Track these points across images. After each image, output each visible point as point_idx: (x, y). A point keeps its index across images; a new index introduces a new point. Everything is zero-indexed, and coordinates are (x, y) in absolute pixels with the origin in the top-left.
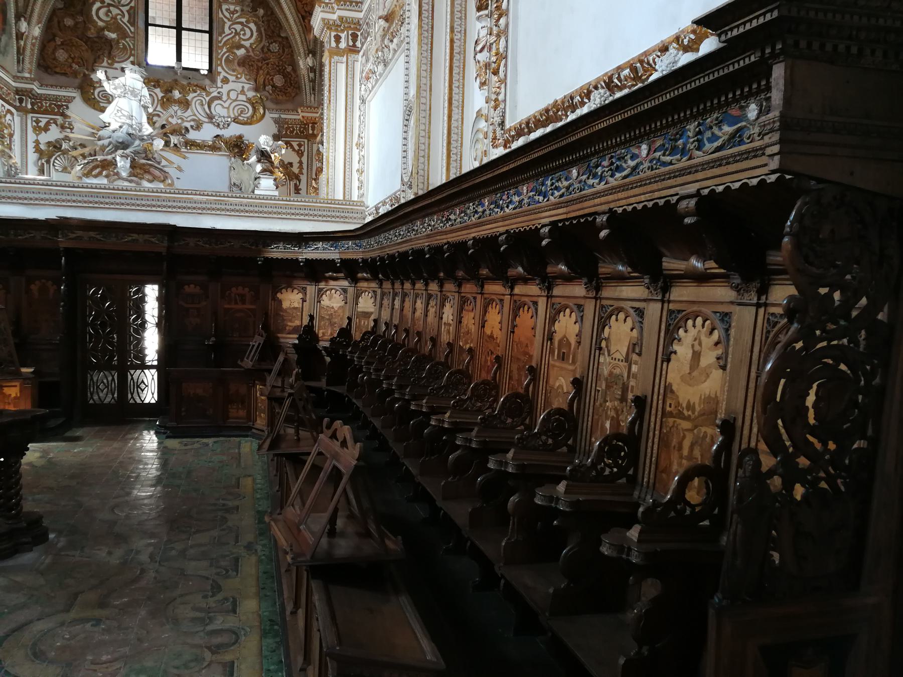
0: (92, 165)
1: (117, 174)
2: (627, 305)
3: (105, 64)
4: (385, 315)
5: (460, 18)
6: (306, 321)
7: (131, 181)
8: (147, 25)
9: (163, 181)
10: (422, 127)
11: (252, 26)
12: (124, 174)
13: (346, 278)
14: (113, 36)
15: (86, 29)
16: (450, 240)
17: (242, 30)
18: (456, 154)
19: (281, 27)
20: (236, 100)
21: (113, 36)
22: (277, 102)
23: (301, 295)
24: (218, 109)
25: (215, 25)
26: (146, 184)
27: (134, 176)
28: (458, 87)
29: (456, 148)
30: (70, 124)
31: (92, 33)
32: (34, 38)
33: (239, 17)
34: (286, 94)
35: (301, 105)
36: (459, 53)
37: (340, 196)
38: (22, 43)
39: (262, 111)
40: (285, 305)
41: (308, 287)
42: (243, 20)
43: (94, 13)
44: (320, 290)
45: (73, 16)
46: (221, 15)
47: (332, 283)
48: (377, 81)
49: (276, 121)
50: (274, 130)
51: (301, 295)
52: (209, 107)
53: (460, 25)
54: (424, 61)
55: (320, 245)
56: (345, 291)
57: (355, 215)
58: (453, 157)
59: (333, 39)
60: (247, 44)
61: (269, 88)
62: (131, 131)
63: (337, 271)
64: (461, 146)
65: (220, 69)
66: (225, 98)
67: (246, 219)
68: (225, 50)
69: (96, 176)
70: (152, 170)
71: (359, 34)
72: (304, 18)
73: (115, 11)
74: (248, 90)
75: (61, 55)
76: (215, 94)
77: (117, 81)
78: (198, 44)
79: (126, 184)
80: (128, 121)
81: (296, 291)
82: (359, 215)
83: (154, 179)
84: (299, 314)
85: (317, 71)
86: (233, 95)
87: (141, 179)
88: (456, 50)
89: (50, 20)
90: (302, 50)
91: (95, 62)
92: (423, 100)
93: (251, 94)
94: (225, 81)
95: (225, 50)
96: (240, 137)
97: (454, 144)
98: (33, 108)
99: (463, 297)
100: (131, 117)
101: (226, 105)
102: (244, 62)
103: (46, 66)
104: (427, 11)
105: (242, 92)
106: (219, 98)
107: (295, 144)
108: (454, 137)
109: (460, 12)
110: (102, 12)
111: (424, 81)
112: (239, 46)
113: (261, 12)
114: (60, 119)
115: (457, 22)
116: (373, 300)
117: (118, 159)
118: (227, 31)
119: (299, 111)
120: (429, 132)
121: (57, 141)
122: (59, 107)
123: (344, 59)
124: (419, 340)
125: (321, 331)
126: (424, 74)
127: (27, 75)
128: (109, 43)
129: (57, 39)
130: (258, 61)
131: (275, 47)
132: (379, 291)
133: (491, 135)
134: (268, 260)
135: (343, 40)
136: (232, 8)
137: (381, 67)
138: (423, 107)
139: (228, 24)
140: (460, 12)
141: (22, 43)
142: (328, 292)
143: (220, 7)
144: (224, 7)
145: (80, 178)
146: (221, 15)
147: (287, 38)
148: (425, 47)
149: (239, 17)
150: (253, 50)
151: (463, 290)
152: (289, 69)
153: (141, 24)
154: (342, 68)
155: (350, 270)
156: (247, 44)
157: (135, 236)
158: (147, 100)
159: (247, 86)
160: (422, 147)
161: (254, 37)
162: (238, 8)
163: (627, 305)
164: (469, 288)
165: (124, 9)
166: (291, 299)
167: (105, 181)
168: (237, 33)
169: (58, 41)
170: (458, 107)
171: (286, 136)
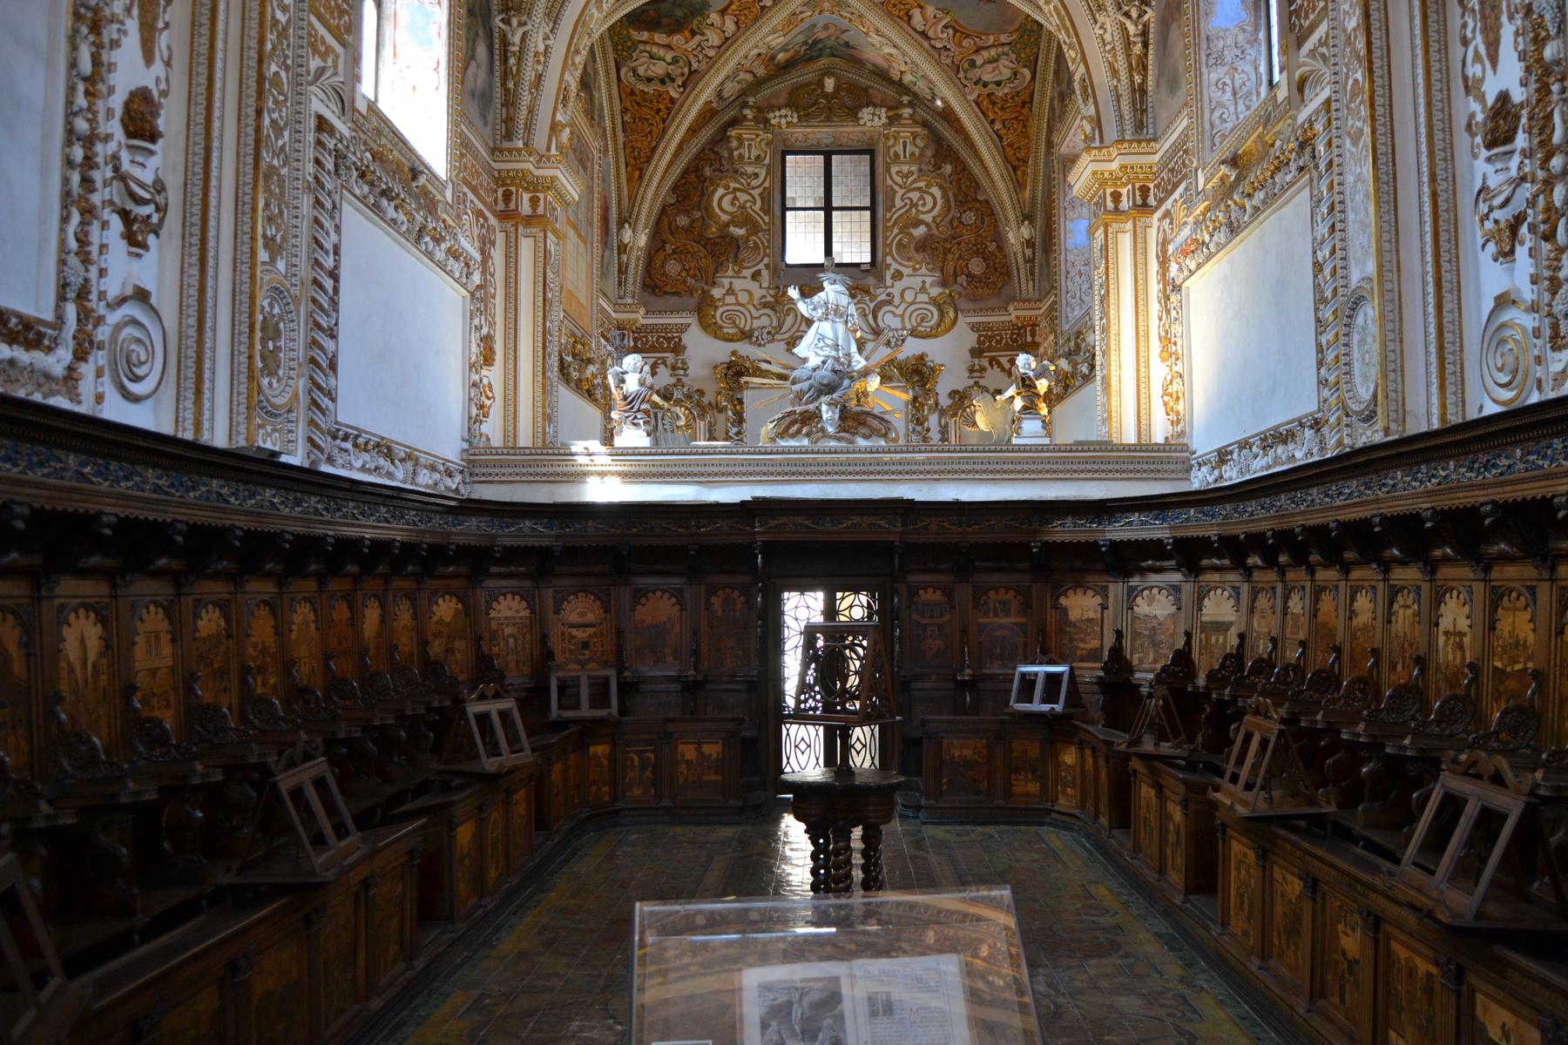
0: (788, 420)
1: (823, 430)
2: (1366, 584)
3: (730, 272)
4: (1263, 626)
5: (1445, 159)
6: (1180, 644)
7: (839, 440)
8: (784, 209)
9: (885, 436)
10: (1390, 326)
11: (936, 191)
12: (830, 430)
13: (1177, 569)
14: (741, 232)
15: (705, 226)
16: (1497, 498)
17: (922, 198)
18: (1454, 363)
19: (978, 186)
20: (913, 303)
21: (741, 232)
22: (974, 298)
23: (1098, 599)
24: (888, 320)
25: (880, 198)
26: (862, 442)
27: (845, 431)
28: (1450, 261)
29: (1453, 353)
30: (684, 363)
31: (713, 231)
32: (639, 249)
33: (915, 181)
34: (987, 285)
35: (1013, 299)
36: (1447, 211)
37: (1131, 438)
38: (625, 257)
39: (952, 314)
40: (1074, 615)
41: (1112, 587)
42: (922, 184)
43: (715, 204)
44: (1131, 590)
45: (687, 213)
46: (889, 182)
47: (1154, 578)
48: (1208, 259)
49: (974, 328)
50: (972, 340)
51: (1098, 599)
52: (875, 318)
53: (1445, 170)
54: (1386, 227)
55: (1135, 517)
56: (1175, 589)
57: (1172, 467)
58: (1450, 368)
59: (1109, 199)
60: (928, 218)
61: (962, 279)
62: (838, 367)
63: (1166, 556)
64: (1461, 350)
65: (889, 260)
66: (897, 301)
67: (1005, 484)
68: (896, 231)
69: (793, 436)
70: (869, 419)
71: (1151, 186)
72: (1015, 169)
73: (743, 197)
74: (932, 285)
75: (673, 268)
76: (883, 297)
77: (816, 299)
78: (856, 227)
79: (833, 443)
80: (833, 353)
81: (1090, 593)
82: (1179, 467)
83: (873, 433)
84: (1098, 629)
85: (1047, 242)
86: (909, 296)
87: (853, 434)
88: (1442, 206)
89: (658, 222)
90: (1012, 216)
91: (716, 271)
92: (1388, 286)
93: (935, 291)
94: (898, 276)
95: (896, 231)
96: (922, 357)
97: (1449, 348)
98: (635, 346)
99: (1391, 587)
100: (836, 347)
101: (899, 311)
102: (924, 245)
103: (654, 285)
104: (1385, 154)
105: (923, 290)
106: (889, 302)
107: (1004, 361)
108: (1448, 337)
109: (1444, 150)
110: (728, 198)
111: (1387, 256)
112: (917, 223)
113: (948, 168)
114: (670, 357)
115: (1441, 165)
116: (1232, 601)
117: (824, 408)
118: (898, 203)
119: (1011, 308)
120: (1401, 333)
121: (666, 388)
122: (669, 340)
123: (1129, 226)
124: (1376, 663)
125: (1136, 656)
126: (1387, 246)
127: (629, 301)
128: (735, 243)
129: (668, 246)
130: (946, 240)
131: (970, 217)
132: (1245, 588)
133: (1547, 332)
134: (1047, 546)
135: (1124, 198)
136: (905, 169)
137: (1220, 237)
138: (1388, 296)
139: (901, 192)
140: (1444, 150)
141: (625, 257)
142: (1146, 593)
143: (888, 170)
144: (894, 170)
145: (773, 440)
146: (889, 182)
147: (987, 202)
148: (1385, 207)
149: (915, 181)
150: (938, 226)
151: (1439, 576)
152: (992, 247)
153: (778, 212)
154: (1126, 241)
155: (1189, 555)
156: (928, 218)
157: (857, 519)
158: (856, 319)
159: (929, 280)
160: (1392, 356)
161: (938, 207)
162: (913, 169)
163: (1366, 584)
164: (1326, 575)
165: (756, 193)
166: (1081, 605)
167: (806, 442)
168: (913, 205)
169: (669, 248)
170: (1451, 291)
171: (991, 349)
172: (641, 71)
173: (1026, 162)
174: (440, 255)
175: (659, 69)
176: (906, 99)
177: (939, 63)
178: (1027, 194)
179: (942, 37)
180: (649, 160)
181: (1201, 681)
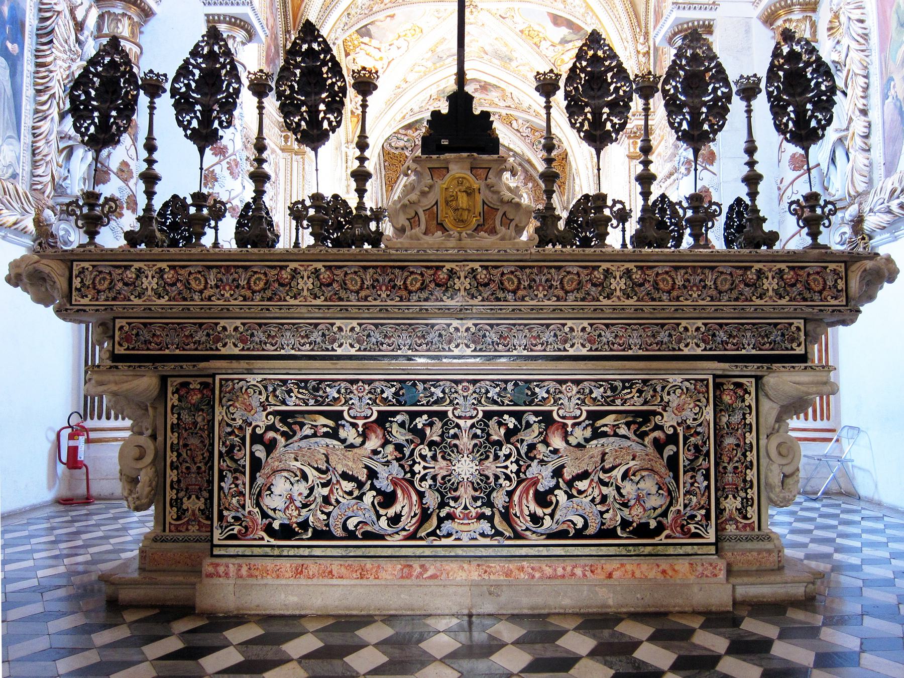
113: (530, 185)
172: (393, 144)
173: (564, 183)
174: (408, 32)
175: (401, 144)
176: (511, 153)
177: (524, 141)
178: (565, 198)
179: (527, 132)
180: (396, 182)
181: (354, 212)
